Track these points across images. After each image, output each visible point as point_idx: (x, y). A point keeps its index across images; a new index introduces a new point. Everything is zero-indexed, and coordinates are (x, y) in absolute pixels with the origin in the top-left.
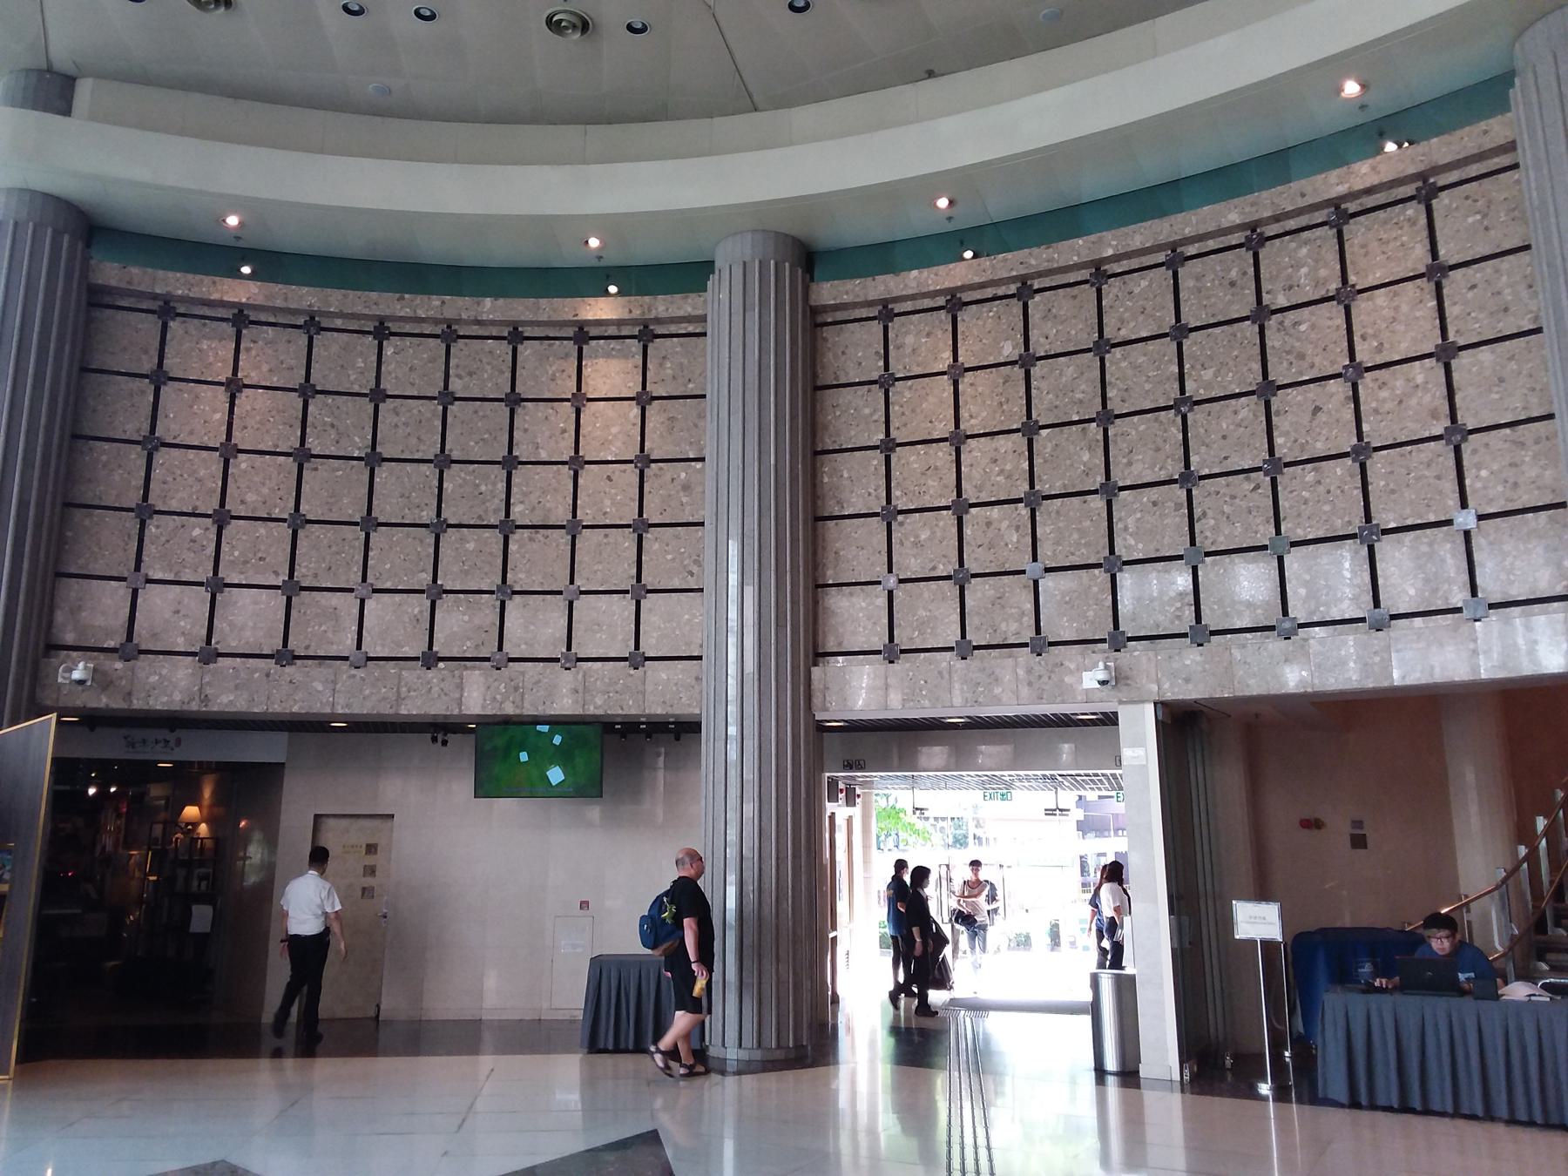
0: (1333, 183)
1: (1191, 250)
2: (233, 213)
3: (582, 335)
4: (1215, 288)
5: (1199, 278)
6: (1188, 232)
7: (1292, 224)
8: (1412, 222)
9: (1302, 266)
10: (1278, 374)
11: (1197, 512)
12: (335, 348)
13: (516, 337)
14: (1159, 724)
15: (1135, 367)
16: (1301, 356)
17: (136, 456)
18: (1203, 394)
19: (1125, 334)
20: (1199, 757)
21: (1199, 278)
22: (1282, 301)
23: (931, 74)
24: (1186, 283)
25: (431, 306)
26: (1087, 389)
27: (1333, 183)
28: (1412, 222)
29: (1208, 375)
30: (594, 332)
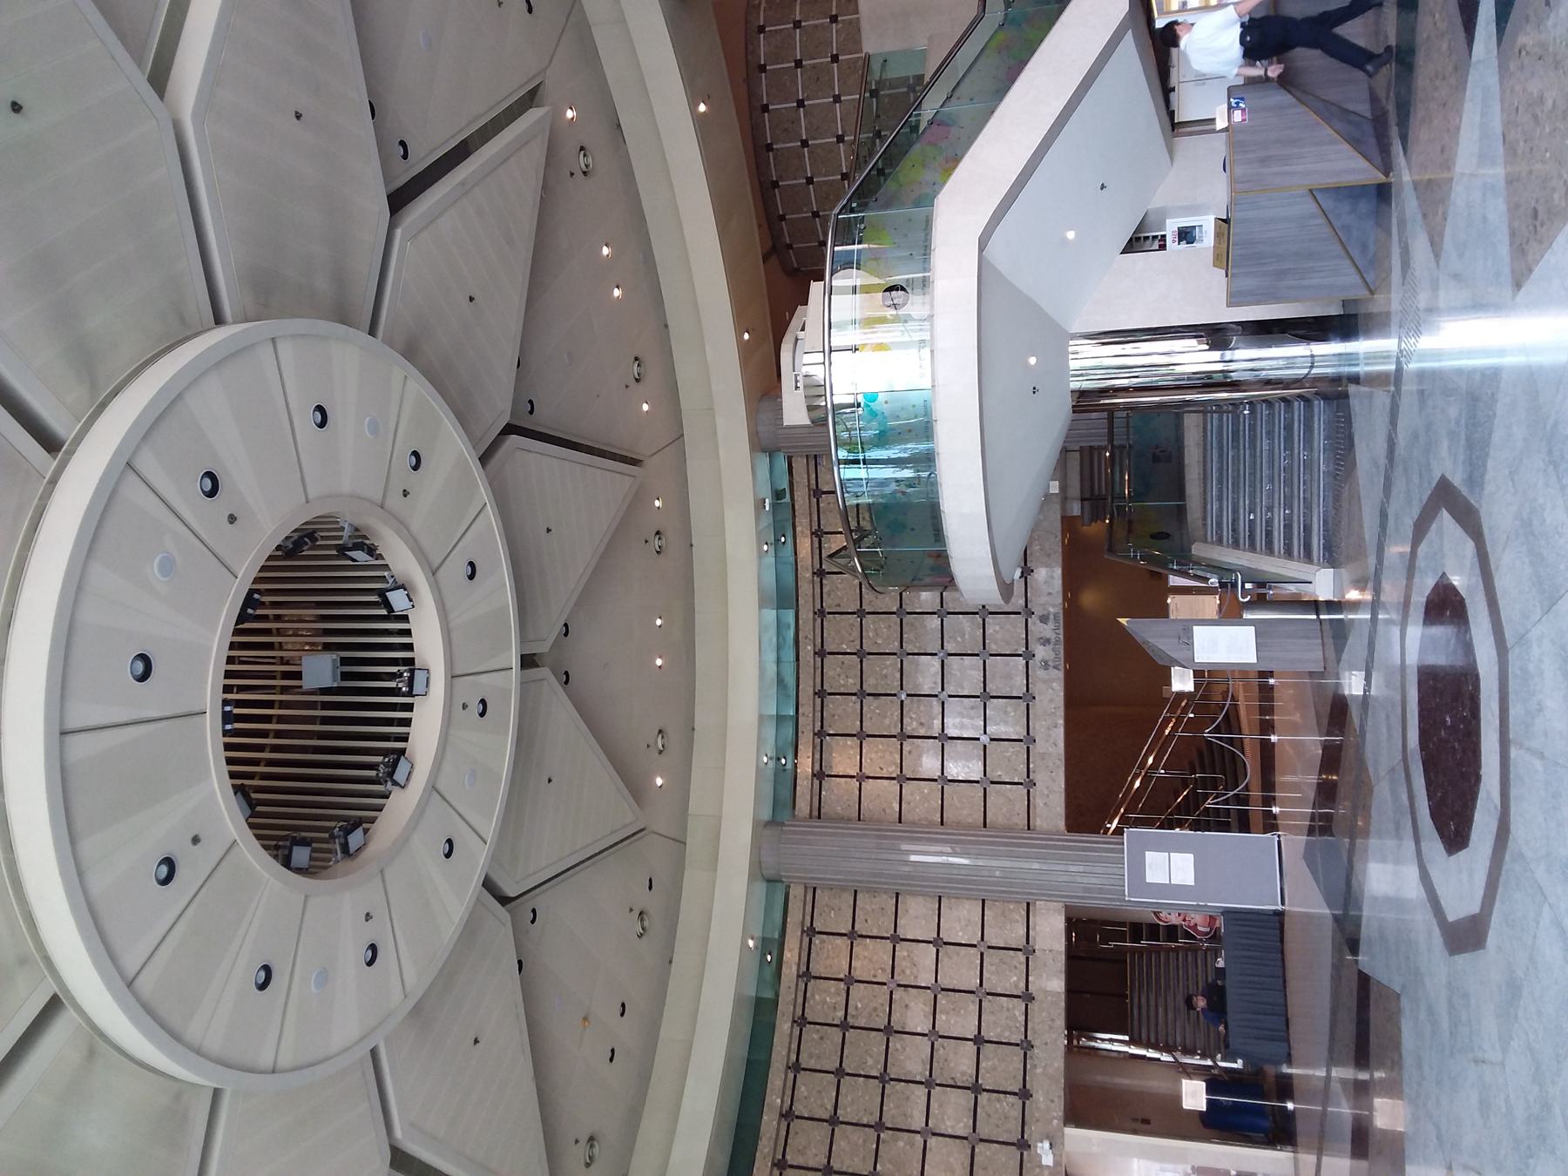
0: (790, 971)
1: (794, 1057)
3: (820, 775)
4: (821, 1049)
5: (811, 1056)
6: (784, 1053)
7: (800, 1000)
8: (823, 942)
9: (825, 1001)
10: (881, 1022)
11: (951, 1082)
12: (994, 978)
14: (1078, 1126)
15: (853, 1102)
16: (875, 1009)
18: (881, 1066)
19: (830, 1107)
20: (1161, 1001)
21: (811, 1056)
22: (841, 1014)
23: (619, 126)
24: (812, 1064)
26: (857, 1136)
27: (790, 971)
28: (823, 942)
29: (870, 1062)
30: (817, 767)
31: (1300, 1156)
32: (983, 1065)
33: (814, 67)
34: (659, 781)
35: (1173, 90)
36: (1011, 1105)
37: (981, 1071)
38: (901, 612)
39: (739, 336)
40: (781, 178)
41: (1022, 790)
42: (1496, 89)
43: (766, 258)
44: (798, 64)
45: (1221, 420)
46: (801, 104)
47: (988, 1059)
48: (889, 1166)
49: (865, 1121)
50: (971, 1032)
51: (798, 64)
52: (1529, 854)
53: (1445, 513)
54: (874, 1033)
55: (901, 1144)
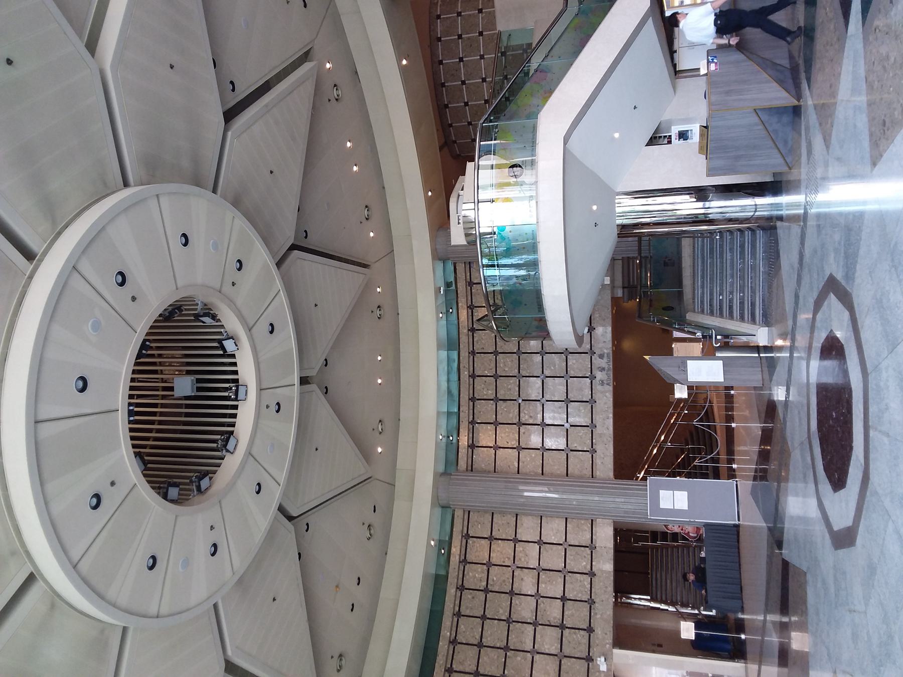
0: (455, 559)
1: (457, 609)
2: (591, 209)
3: (472, 446)
4: (473, 604)
5: (467, 608)
6: (452, 606)
7: (461, 576)
8: (474, 542)
9: (475, 576)
10: (507, 589)
11: (548, 623)
13: (458, 615)
14: (621, 648)
15: (491, 635)
16: (504, 581)
17: (500, 452)
18: (507, 614)
19: (478, 637)
21: (467, 608)
22: (484, 584)
24: (468, 613)
25: (447, 621)
26: (494, 654)
27: (455, 559)
28: (474, 542)
29: (501, 611)
30: (471, 442)
31: (749, 665)
32: (566, 613)
33: (469, 38)
34: (380, 450)
35: (676, 52)
36: (582, 636)
37: (565, 617)
38: (519, 352)
39: (426, 193)
40: (450, 102)
41: (589, 455)
42: (861, 51)
43: (441, 149)
44: (460, 37)
45: (703, 242)
46: (461, 60)
47: (569, 610)
48: (512, 671)
49: (498, 645)
50: (559, 594)
51: (460, 37)
52: (880, 492)
53: (832, 295)
54: (503, 595)
55: (519, 658)
